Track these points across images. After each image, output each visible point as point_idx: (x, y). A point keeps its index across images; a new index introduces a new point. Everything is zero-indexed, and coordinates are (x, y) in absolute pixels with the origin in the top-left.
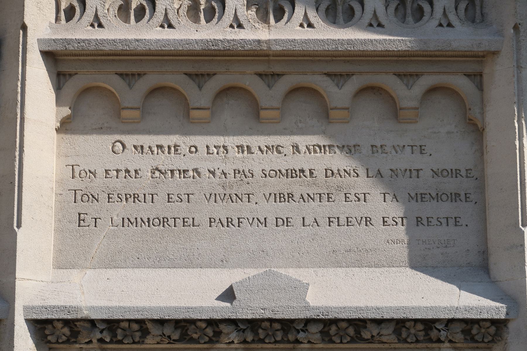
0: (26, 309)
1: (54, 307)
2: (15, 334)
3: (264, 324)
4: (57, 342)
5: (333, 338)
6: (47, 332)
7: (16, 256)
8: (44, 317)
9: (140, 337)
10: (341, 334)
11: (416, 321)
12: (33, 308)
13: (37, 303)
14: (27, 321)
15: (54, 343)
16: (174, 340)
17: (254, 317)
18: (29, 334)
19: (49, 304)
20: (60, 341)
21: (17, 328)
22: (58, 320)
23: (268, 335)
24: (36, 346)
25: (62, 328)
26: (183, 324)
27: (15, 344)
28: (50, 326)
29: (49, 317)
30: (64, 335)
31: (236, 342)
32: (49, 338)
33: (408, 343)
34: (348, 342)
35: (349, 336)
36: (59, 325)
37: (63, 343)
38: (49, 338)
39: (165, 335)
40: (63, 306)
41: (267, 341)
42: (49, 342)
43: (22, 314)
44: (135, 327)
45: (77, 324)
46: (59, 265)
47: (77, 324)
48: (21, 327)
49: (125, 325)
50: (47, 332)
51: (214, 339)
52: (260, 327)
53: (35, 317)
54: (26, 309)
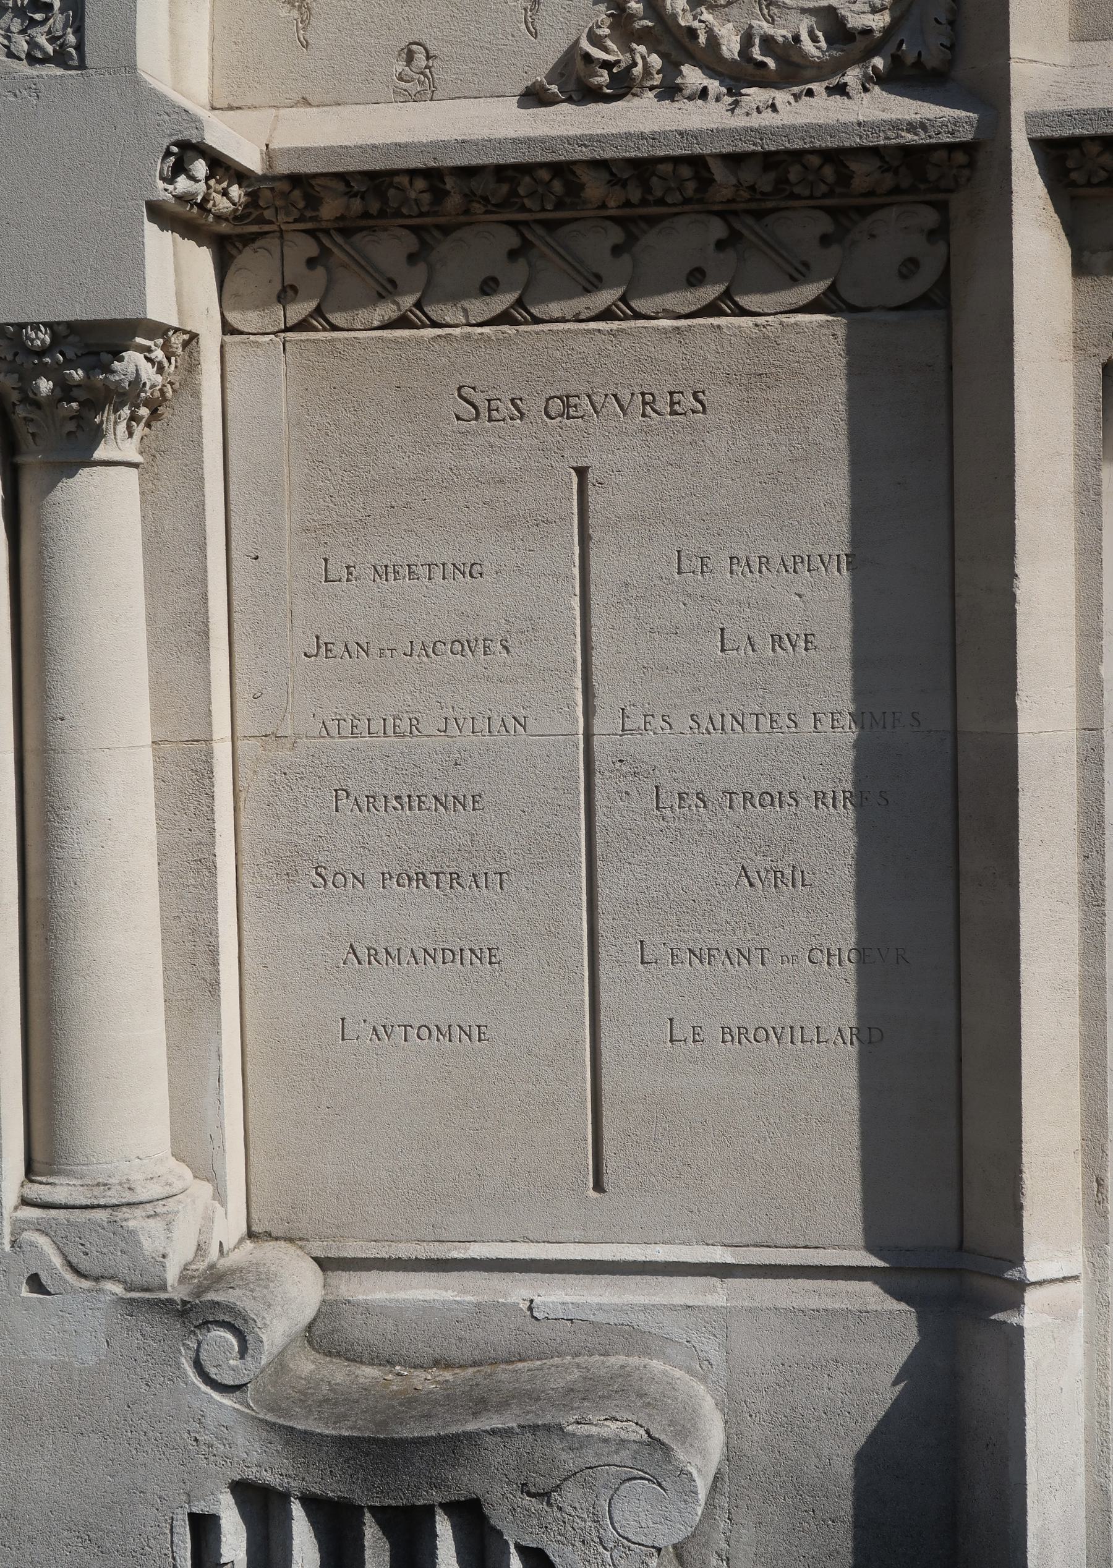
0: (1030, 117)
1: (1086, 112)
2: (1013, 167)
3: (937, 156)
4: (1089, 184)
5: (526, 201)
6: (1071, 164)
7: (1008, 13)
8: (1066, 133)
9: (696, 191)
10: (811, 177)
11: (413, 173)
12: (1045, 115)
13: (1051, 106)
14: (1034, 143)
15: (1082, 186)
16: (494, 205)
17: (824, 145)
18: (1036, 168)
19: (1075, 107)
20: (1095, 180)
21: (1015, 156)
22: (1093, 138)
23: (668, 190)
24: (1050, 192)
25: (1098, 155)
26: (510, 173)
27: (1014, 188)
28: (1076, 152)
29: (1077, 132)
30: (1103, 169)
31: (612, 203)
32: (1074, 175)
33: (403, 216)
34: (824, 196)
35: (824, 182)
36: (1095, 149)
37: (1100, 184)
38: (1074, 175)
39: (475, 195)
40: (1103, 109)
41: (669, 200)
42: (1073, 184)
43: (1024, 129)
44: (420, 184)
45: (574, 168)
46: (1082, 34)
47: (319, 181)
48: (1022, 154)
49: (939, 156)
50: (1071, 164)
51: (568, 200)
52: (653, 174)
53: (1048, 133)
54: (1030, 117)
